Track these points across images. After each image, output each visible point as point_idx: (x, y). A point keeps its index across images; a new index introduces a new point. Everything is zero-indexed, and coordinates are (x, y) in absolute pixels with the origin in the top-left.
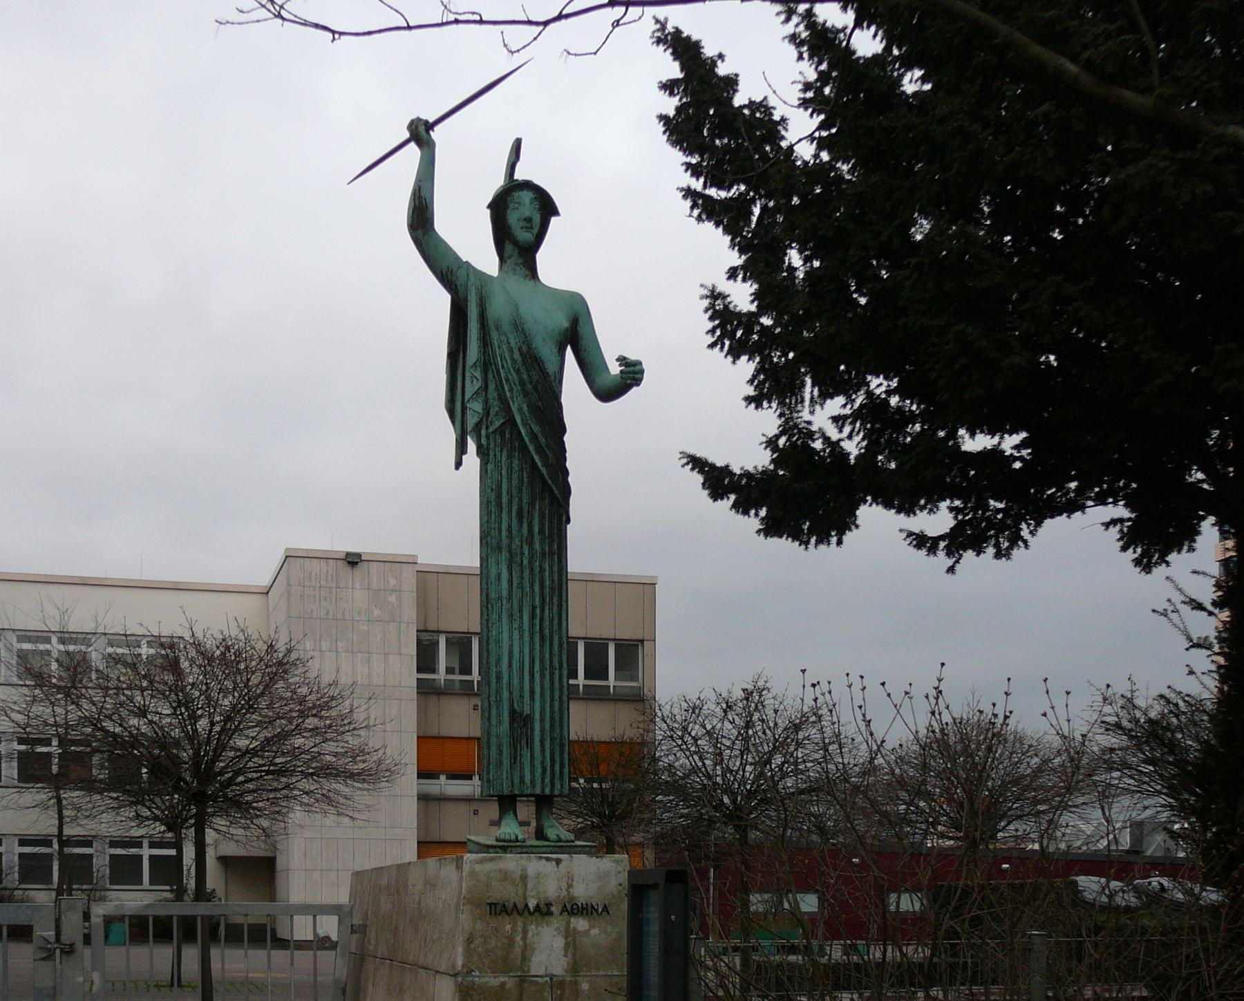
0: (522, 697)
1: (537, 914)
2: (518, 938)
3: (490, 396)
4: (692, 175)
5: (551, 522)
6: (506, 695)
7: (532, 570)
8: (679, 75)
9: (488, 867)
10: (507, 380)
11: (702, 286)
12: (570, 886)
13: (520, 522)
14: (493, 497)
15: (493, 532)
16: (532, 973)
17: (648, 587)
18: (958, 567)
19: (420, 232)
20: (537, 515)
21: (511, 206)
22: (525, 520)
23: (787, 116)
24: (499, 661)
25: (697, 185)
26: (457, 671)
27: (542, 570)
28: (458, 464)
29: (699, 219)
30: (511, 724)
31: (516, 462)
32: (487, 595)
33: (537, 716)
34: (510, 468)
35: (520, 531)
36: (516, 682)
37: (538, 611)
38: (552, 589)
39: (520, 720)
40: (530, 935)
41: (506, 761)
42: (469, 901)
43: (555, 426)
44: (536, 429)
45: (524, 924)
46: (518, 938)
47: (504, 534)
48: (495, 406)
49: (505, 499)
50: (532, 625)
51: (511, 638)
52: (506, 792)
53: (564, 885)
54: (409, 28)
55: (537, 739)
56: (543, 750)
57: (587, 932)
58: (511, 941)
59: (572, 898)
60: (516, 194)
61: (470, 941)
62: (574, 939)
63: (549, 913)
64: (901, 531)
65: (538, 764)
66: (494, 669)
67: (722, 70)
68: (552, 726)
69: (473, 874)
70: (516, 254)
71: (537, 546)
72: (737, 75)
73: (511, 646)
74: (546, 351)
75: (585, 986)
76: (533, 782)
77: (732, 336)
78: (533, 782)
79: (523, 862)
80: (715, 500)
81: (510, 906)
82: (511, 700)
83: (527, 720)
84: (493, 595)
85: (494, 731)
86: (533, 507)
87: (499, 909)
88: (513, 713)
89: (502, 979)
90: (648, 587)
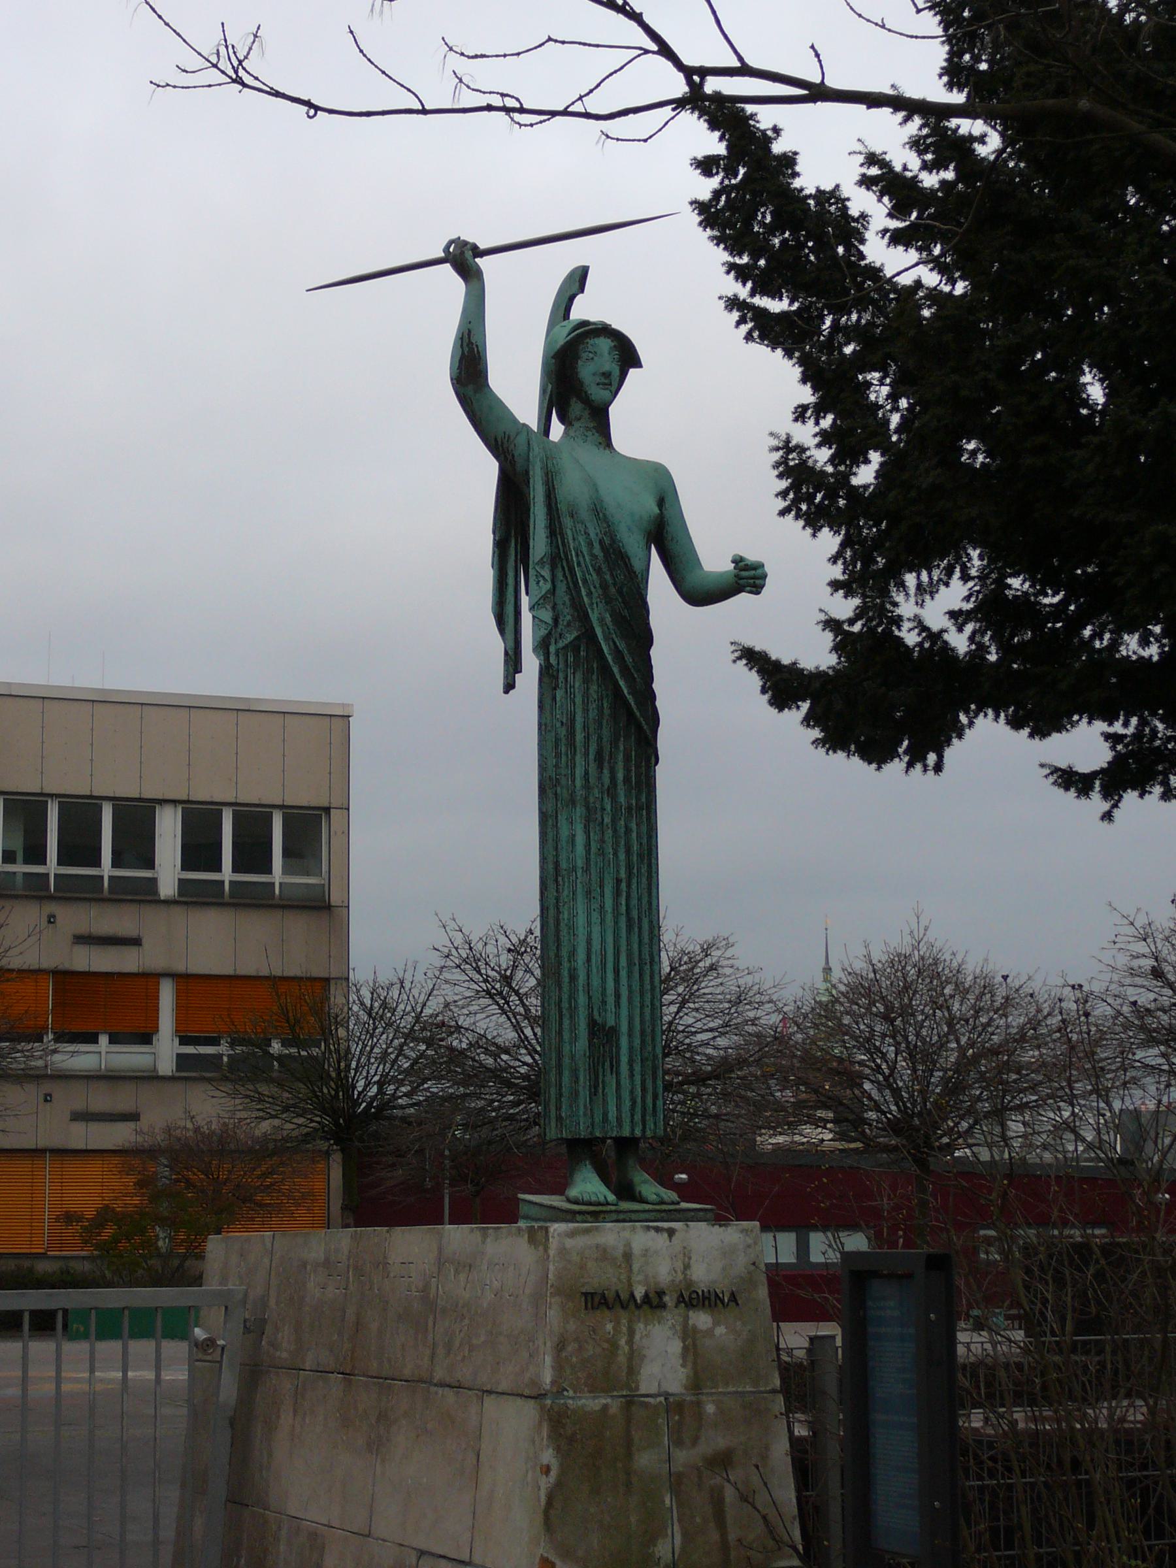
0: (604, 1002)
1: (646, 1307)
2: (623, 1342)
3: (559, 602)
4: (737, 279)
5: (638, 767)
6: (582, 999)
7: (615, 831)
8: (721, 149)
9: (580, 1242)
10: (585, 581)
11: (771, 434)
12: (687, 1267)
13: (600, 767)
14: (563, 732)
15: (563, 782)
16: (642, 1391)
17: (338, 722)
18: (1116, 813)
19: (469, 391)
20: (621, 757)
21: (584, 355)
22: (606, 764)
23: (869, 212)
24: (573, 953)
25: (743, 291)
26: (20, 856)
27: (628, 831)
28: (509, 686)
29: (749, 337)
30: (591, 1044)
31: (594, 688)
32: (557, 864)
33: (624, 1028)
34: (586, 695)
35: (600, 778)
36: (596, 982)
37: (624, 886)
38: (640, 856)
39: (602, 1036)
40: (637, 1337)
41: (584, 1094)
42: (558, 1292)
43: (642, 638)
44: (622, 645)
45: (630, 1321)
46: (623, 1342)
47: (578, 783)
48: (567, 615)
49: (579, 737)
50: (616, 905)
51: (589, 924)
52: (583, 1135)
53: (679, 1265)
54: (424, 111)
55: (624, 1059)
56: (632, 1076)
57: (709, 1333)
58: (615, 1346)
59: (689, 1283)
60: (591, 342)
61: (560, 1347)
62: (694, 1345)
63: (662, 1306)
64: (1042, 766)
65: (626, 1095)
66: (566, 965)
67: (778, 147)
68: (643, 1042)
69: (563, 1251)
70: (586, 414)
71: (622, 799)
72: (796, 153)
73: (589, 934)
74: (632, 542)
75: (710, 1408)
76: (619, 1120)
77: (810, 499)
78: (619, 1120)
79: (626, 1234)
80: (781, 710)
81: (610, 1295)
82: (590, 1007)
83: (612, 1034)
84: (564, 865)
85: (566, 1049)
86: (617, 747)
87: (598, 1301)
88: (592, 1024)
89: (604, 1401)
90: (338, 722)
